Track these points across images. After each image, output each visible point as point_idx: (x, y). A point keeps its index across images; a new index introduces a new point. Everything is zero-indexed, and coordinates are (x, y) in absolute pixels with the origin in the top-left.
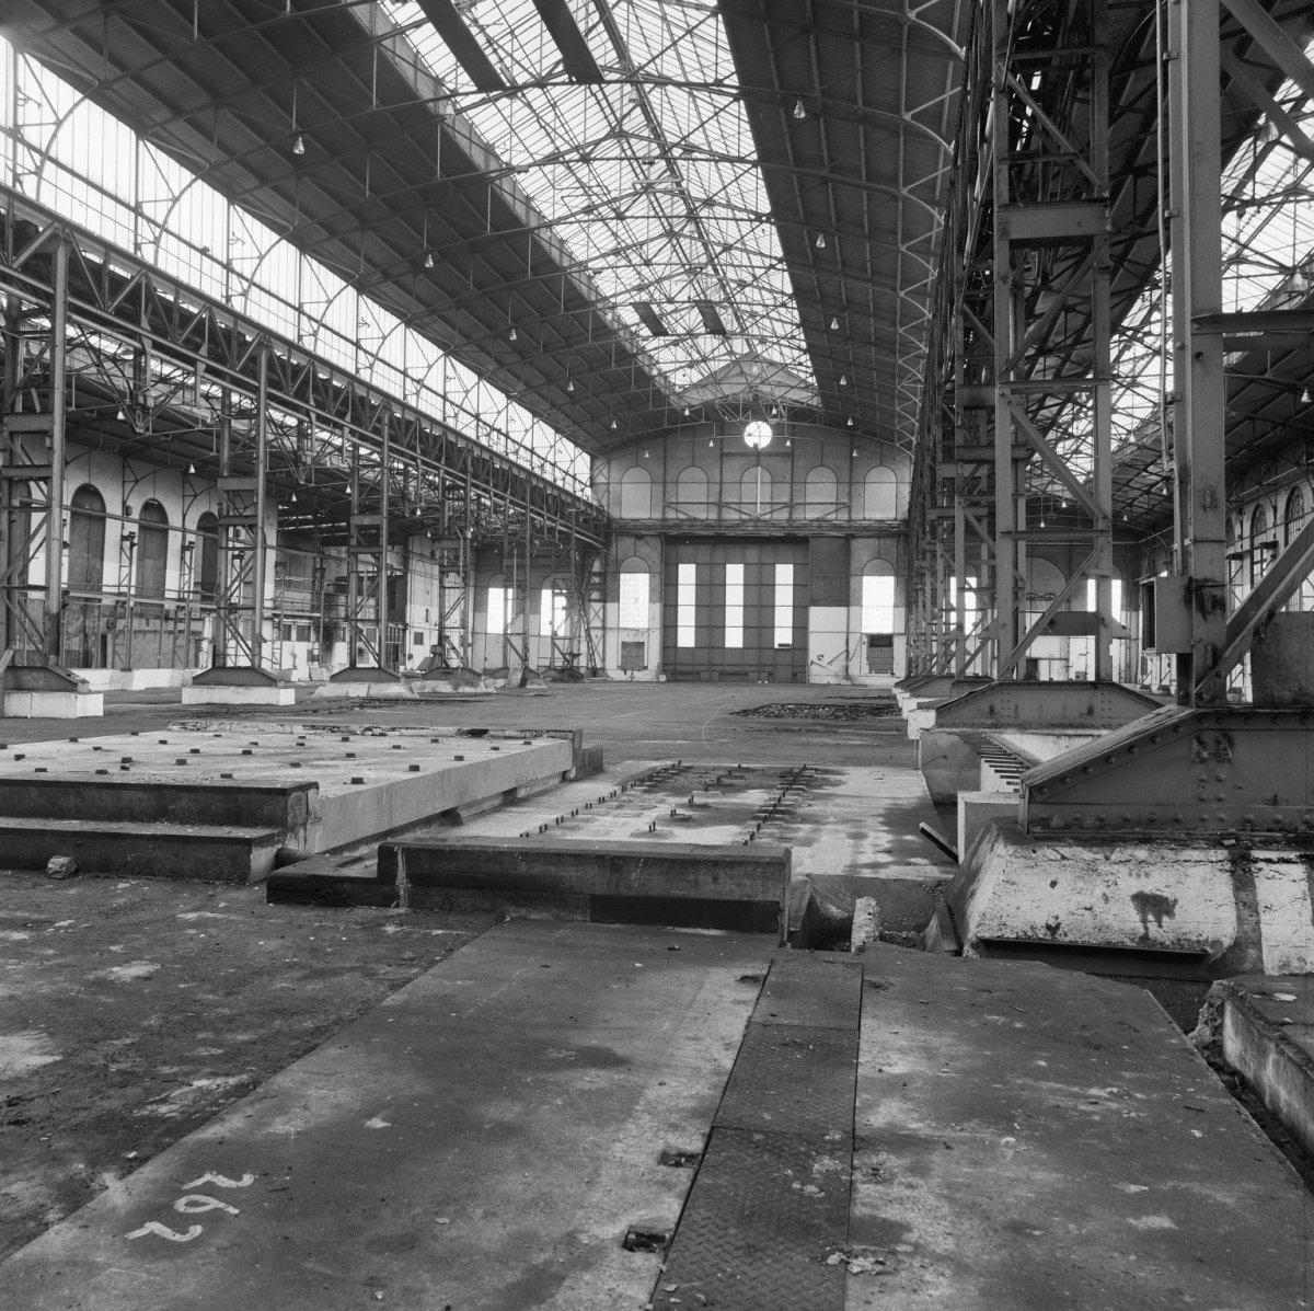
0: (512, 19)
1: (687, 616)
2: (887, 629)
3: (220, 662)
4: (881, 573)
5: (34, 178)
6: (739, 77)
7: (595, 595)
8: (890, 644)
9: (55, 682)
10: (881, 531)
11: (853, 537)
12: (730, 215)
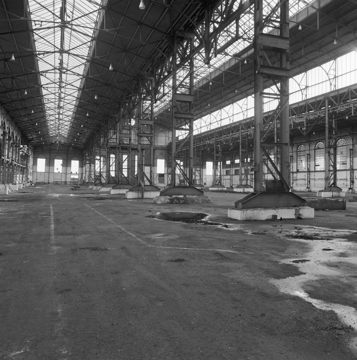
0: (234, 47)
1: (113, 168)
2: (163, 173)
3: (151, 184)
4: (162, 159)
5: (36, 22)
6: (220, 49)
7: (88, 162)
8: (164, 176)
9: (154, 189)
10: (162, 148)
11: (155, 149)
12: (74, 26)
